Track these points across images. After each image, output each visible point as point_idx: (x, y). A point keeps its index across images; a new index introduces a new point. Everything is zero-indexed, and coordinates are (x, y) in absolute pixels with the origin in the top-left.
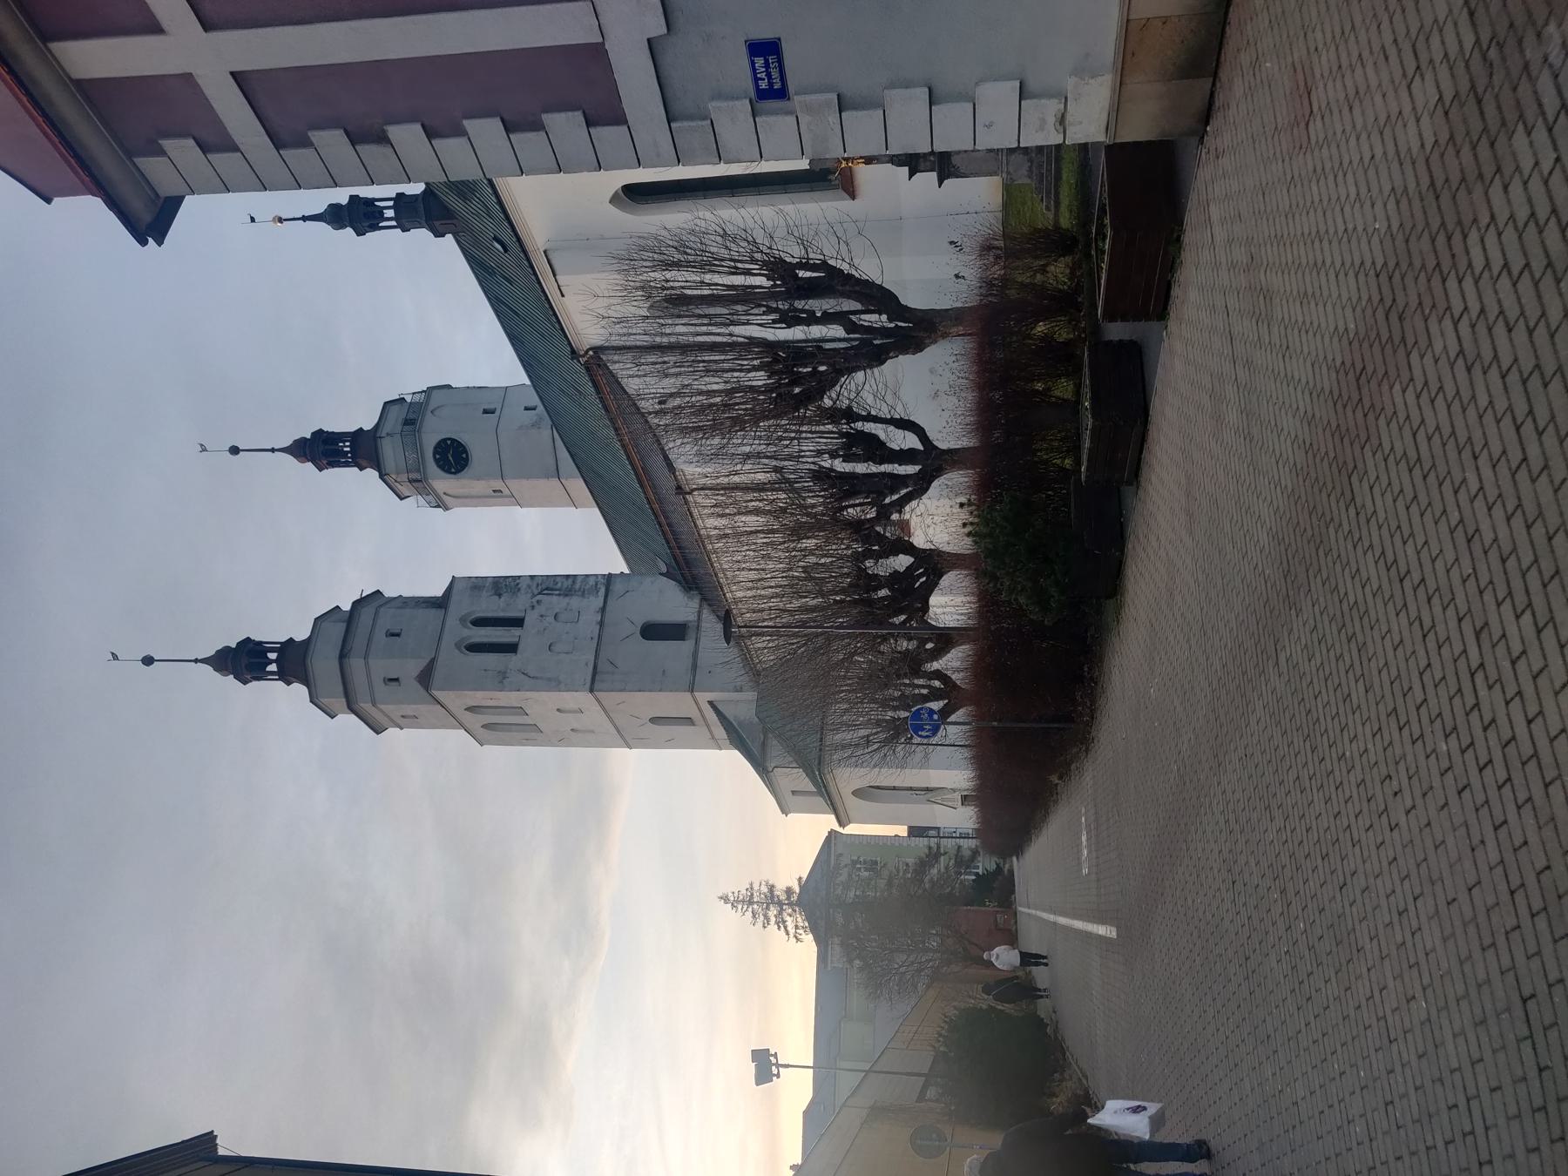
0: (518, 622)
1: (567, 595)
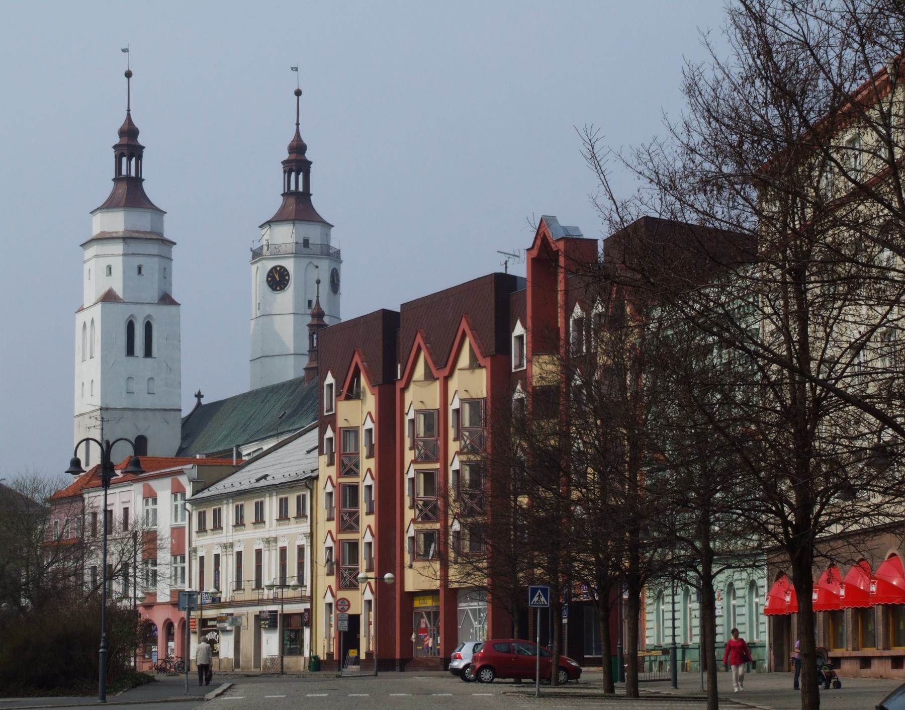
0: (148, 353)
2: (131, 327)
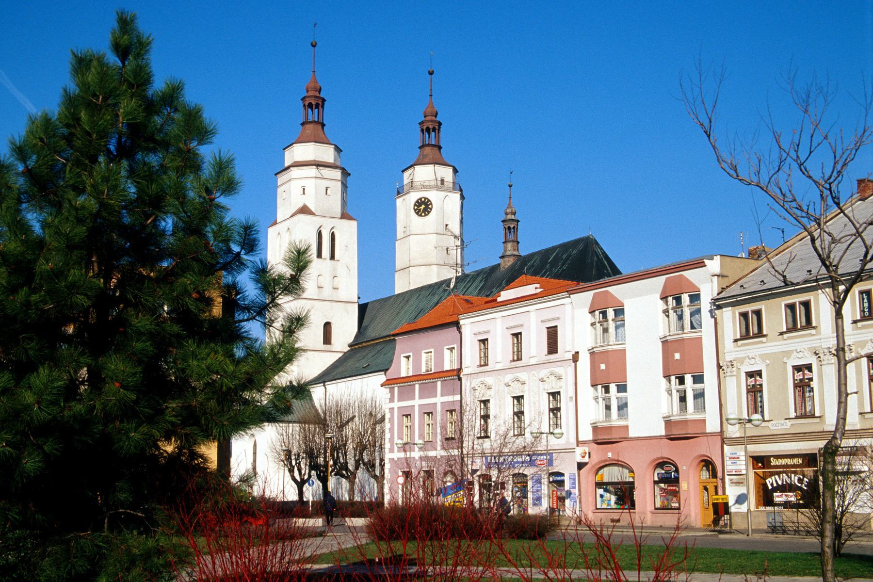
0: (332, 257)
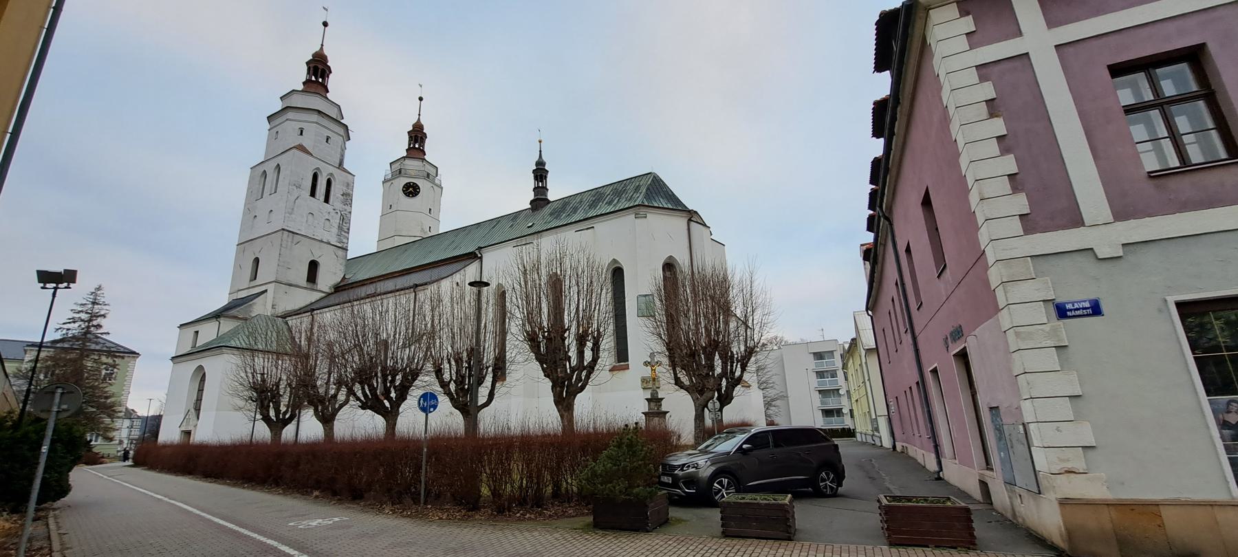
0: (327, 200)
1: (339, 227)
2: (315, 177)
